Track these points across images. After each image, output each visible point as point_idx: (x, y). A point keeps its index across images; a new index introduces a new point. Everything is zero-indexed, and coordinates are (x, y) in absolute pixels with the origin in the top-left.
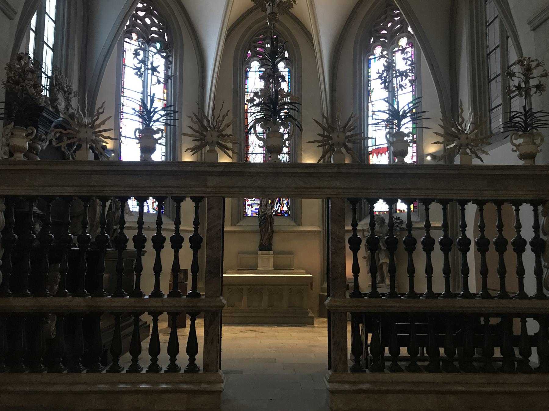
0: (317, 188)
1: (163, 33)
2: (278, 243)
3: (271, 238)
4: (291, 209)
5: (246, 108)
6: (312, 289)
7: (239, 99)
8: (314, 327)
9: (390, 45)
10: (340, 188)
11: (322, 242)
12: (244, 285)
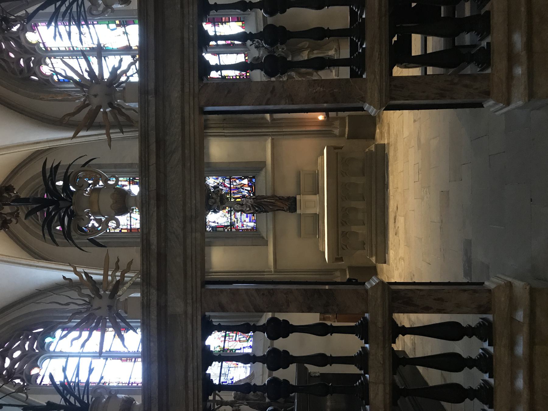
0: (183, 130)
1: (32, 334)
2: (287, 189)
3: (281, 199)
4: (246, 175)
5: (126, 231)
6: (341, 148)
7: (116, 240)
8: (388, 144)
9: (39, 54)
10: (183, 90)
11: (285, 137)
12: (338, 231)
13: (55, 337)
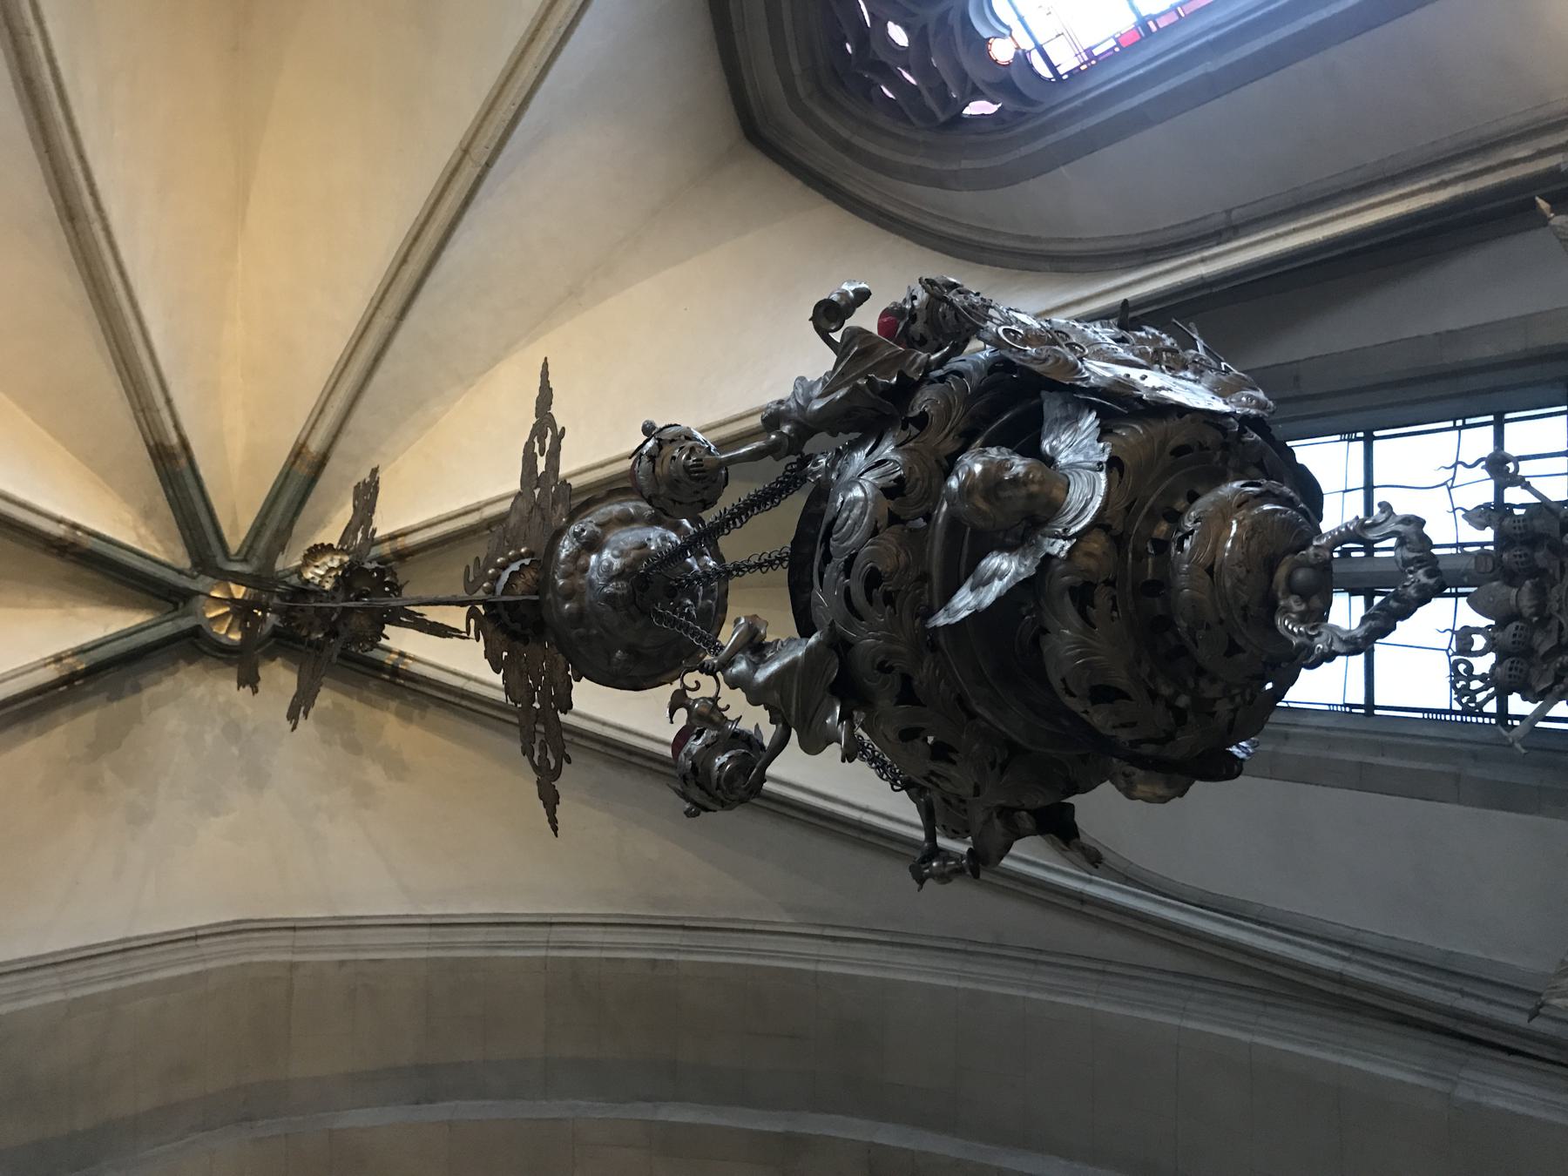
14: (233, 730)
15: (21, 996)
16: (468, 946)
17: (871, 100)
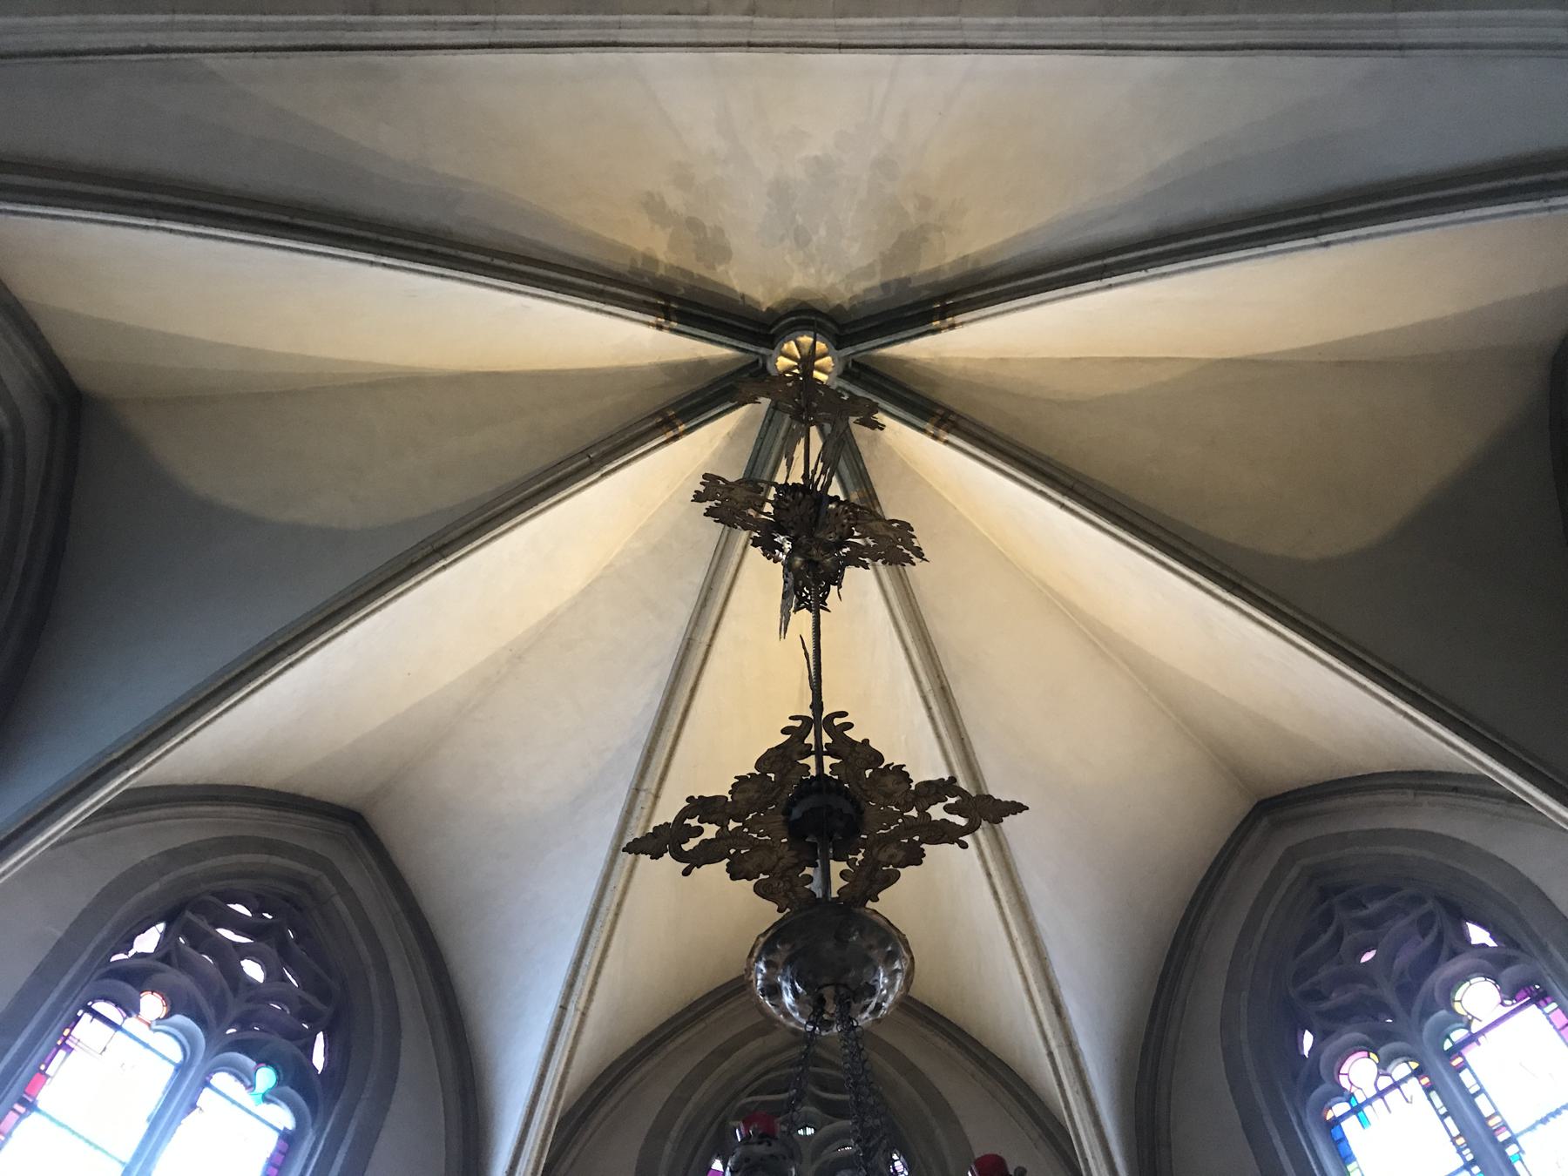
13: (266, 1100)
14: (801, 239)
15: (1000, 28)
16: (581, 24)
17: (258, 897)
